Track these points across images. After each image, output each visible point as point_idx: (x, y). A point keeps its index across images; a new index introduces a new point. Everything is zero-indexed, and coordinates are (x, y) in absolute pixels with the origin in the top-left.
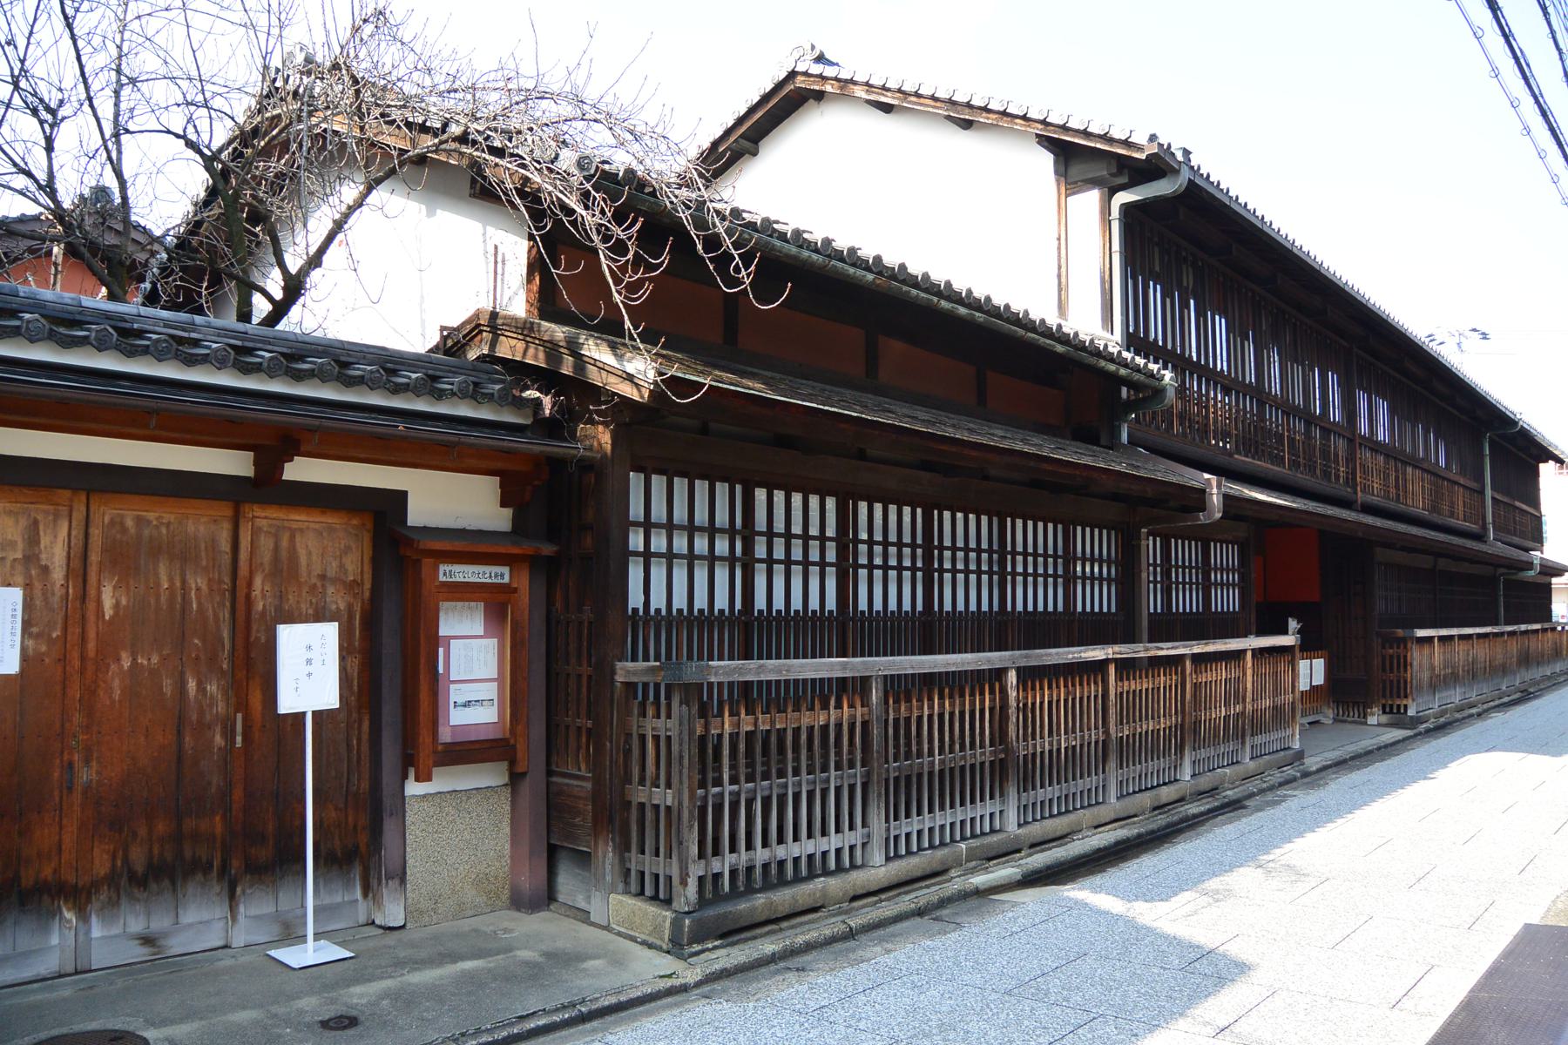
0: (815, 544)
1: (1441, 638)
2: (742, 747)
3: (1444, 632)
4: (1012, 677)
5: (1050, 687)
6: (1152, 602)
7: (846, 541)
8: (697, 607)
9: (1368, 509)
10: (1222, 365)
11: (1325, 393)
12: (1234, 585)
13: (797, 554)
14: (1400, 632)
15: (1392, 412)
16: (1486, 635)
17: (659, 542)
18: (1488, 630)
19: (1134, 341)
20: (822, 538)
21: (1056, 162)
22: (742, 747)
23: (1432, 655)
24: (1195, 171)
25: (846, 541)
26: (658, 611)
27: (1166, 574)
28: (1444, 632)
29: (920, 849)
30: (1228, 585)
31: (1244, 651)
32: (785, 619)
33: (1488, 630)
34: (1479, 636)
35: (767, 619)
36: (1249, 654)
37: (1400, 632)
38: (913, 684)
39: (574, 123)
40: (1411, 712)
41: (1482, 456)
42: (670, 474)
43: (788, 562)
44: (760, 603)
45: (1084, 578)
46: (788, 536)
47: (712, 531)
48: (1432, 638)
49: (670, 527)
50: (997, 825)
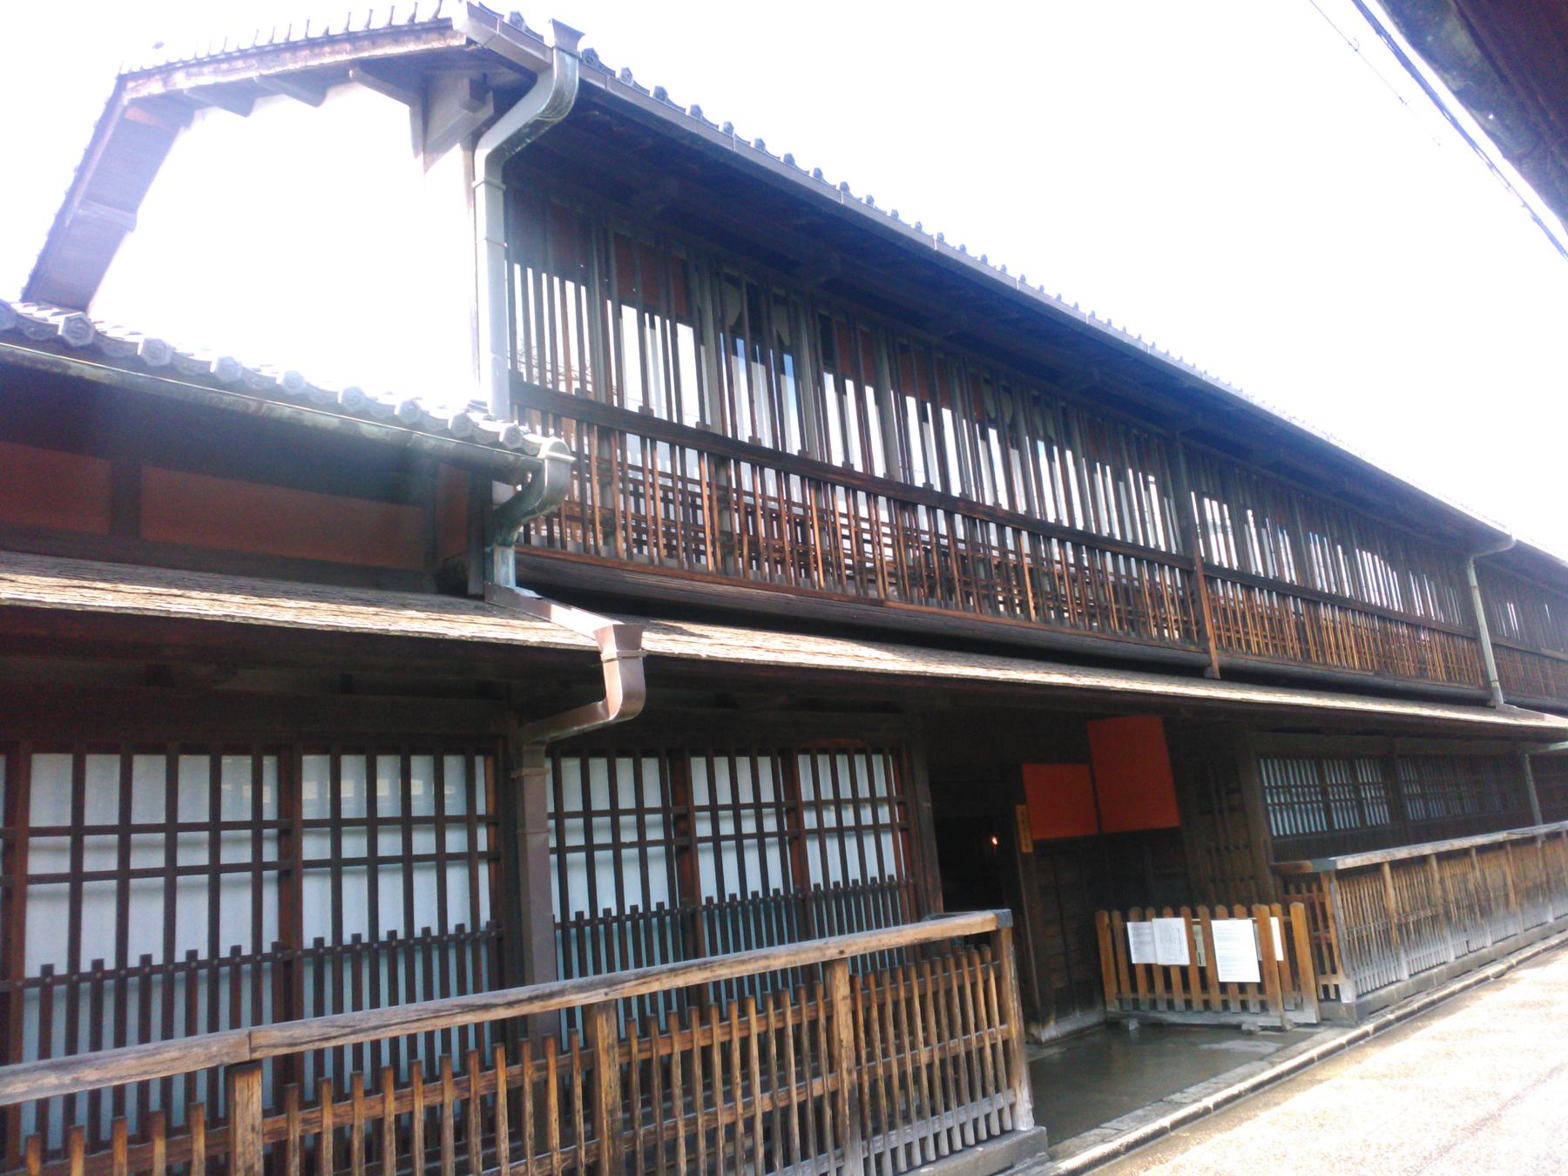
0: (627, 821)
1: (1396, 865)
2: (635, 1078)
3: (1402, 853)
4: (1387, 869)
5: (920, 975)
6: (1415, 811)
7: (790, 807)
8: (750, 890)
9: (1232, 675)
10: (794, 446)
11: (1058, 486)
12: (877, 829)
13: (749, 826)
14: (1309, 865)
15: (699, 340)
16: (1500, 846)
17: (830, 819)
18: (1500, 836)
19: (533, 399)
20: (758, 806)
21: (413, 115)
22: (635, 1078)
23: (1381, 895)
24: (590, 59)
25: (790, 807)
26: (660, 905)
27: (1325, 793)
28: (1402, 853)
29: (952, 1151)
30: (859, 830)
31: (828, 965)
32: (764, 901)
33: (1500, 836)
34: (1482, 849)
35: (719, 906)
36: (1387, 869)
37: (1309, 865)
38: (785, 984)
39: (1458, 642)
40: (1348, 997)
41: (1247, 522)
42: (832, 753)
43: (739, 837)
44: (816, 876)
45: (1274, 804)
46: (736, 807)
47: (874, 802)
48: (1376, 868)
49: (838, 803)
50: (1008, 1126)
